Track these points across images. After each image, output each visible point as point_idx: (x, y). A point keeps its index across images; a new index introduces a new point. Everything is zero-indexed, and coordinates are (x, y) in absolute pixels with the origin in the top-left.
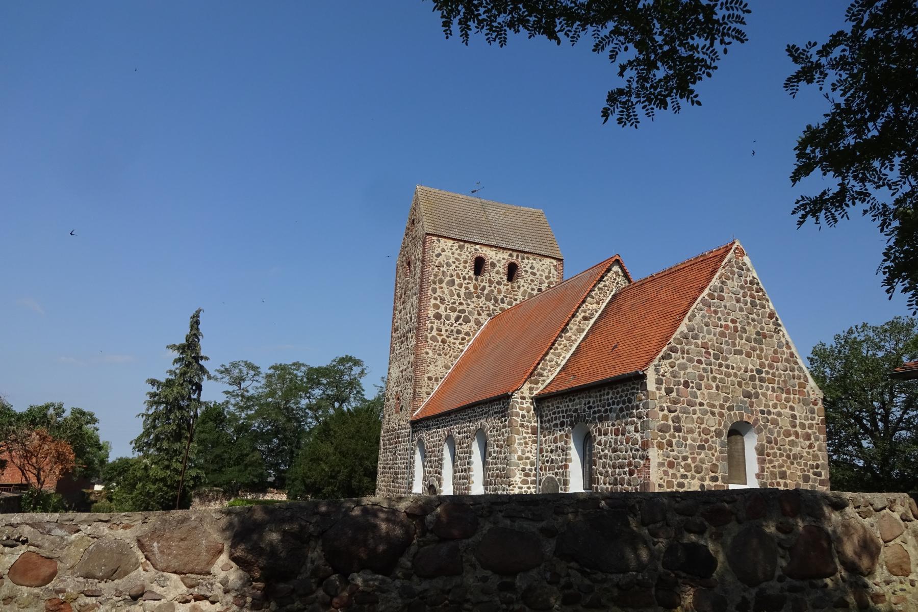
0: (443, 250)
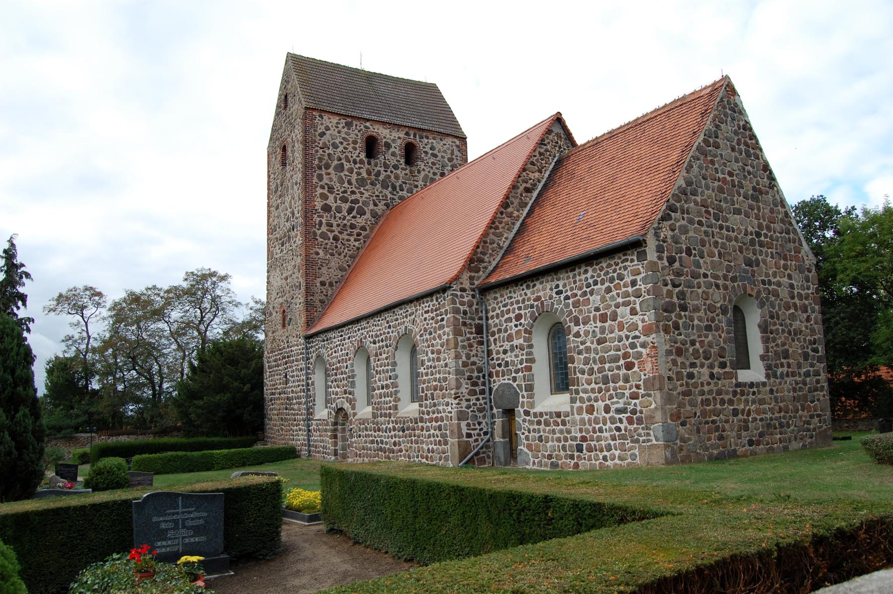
0: (327, 129)
